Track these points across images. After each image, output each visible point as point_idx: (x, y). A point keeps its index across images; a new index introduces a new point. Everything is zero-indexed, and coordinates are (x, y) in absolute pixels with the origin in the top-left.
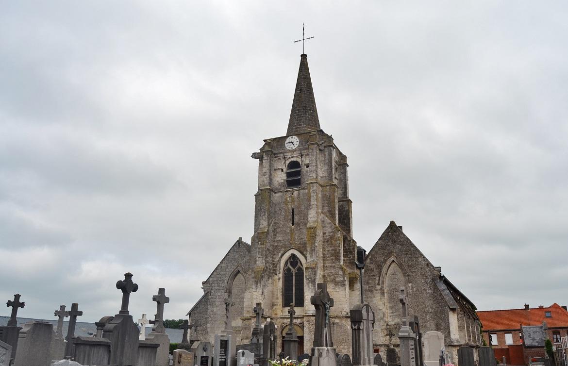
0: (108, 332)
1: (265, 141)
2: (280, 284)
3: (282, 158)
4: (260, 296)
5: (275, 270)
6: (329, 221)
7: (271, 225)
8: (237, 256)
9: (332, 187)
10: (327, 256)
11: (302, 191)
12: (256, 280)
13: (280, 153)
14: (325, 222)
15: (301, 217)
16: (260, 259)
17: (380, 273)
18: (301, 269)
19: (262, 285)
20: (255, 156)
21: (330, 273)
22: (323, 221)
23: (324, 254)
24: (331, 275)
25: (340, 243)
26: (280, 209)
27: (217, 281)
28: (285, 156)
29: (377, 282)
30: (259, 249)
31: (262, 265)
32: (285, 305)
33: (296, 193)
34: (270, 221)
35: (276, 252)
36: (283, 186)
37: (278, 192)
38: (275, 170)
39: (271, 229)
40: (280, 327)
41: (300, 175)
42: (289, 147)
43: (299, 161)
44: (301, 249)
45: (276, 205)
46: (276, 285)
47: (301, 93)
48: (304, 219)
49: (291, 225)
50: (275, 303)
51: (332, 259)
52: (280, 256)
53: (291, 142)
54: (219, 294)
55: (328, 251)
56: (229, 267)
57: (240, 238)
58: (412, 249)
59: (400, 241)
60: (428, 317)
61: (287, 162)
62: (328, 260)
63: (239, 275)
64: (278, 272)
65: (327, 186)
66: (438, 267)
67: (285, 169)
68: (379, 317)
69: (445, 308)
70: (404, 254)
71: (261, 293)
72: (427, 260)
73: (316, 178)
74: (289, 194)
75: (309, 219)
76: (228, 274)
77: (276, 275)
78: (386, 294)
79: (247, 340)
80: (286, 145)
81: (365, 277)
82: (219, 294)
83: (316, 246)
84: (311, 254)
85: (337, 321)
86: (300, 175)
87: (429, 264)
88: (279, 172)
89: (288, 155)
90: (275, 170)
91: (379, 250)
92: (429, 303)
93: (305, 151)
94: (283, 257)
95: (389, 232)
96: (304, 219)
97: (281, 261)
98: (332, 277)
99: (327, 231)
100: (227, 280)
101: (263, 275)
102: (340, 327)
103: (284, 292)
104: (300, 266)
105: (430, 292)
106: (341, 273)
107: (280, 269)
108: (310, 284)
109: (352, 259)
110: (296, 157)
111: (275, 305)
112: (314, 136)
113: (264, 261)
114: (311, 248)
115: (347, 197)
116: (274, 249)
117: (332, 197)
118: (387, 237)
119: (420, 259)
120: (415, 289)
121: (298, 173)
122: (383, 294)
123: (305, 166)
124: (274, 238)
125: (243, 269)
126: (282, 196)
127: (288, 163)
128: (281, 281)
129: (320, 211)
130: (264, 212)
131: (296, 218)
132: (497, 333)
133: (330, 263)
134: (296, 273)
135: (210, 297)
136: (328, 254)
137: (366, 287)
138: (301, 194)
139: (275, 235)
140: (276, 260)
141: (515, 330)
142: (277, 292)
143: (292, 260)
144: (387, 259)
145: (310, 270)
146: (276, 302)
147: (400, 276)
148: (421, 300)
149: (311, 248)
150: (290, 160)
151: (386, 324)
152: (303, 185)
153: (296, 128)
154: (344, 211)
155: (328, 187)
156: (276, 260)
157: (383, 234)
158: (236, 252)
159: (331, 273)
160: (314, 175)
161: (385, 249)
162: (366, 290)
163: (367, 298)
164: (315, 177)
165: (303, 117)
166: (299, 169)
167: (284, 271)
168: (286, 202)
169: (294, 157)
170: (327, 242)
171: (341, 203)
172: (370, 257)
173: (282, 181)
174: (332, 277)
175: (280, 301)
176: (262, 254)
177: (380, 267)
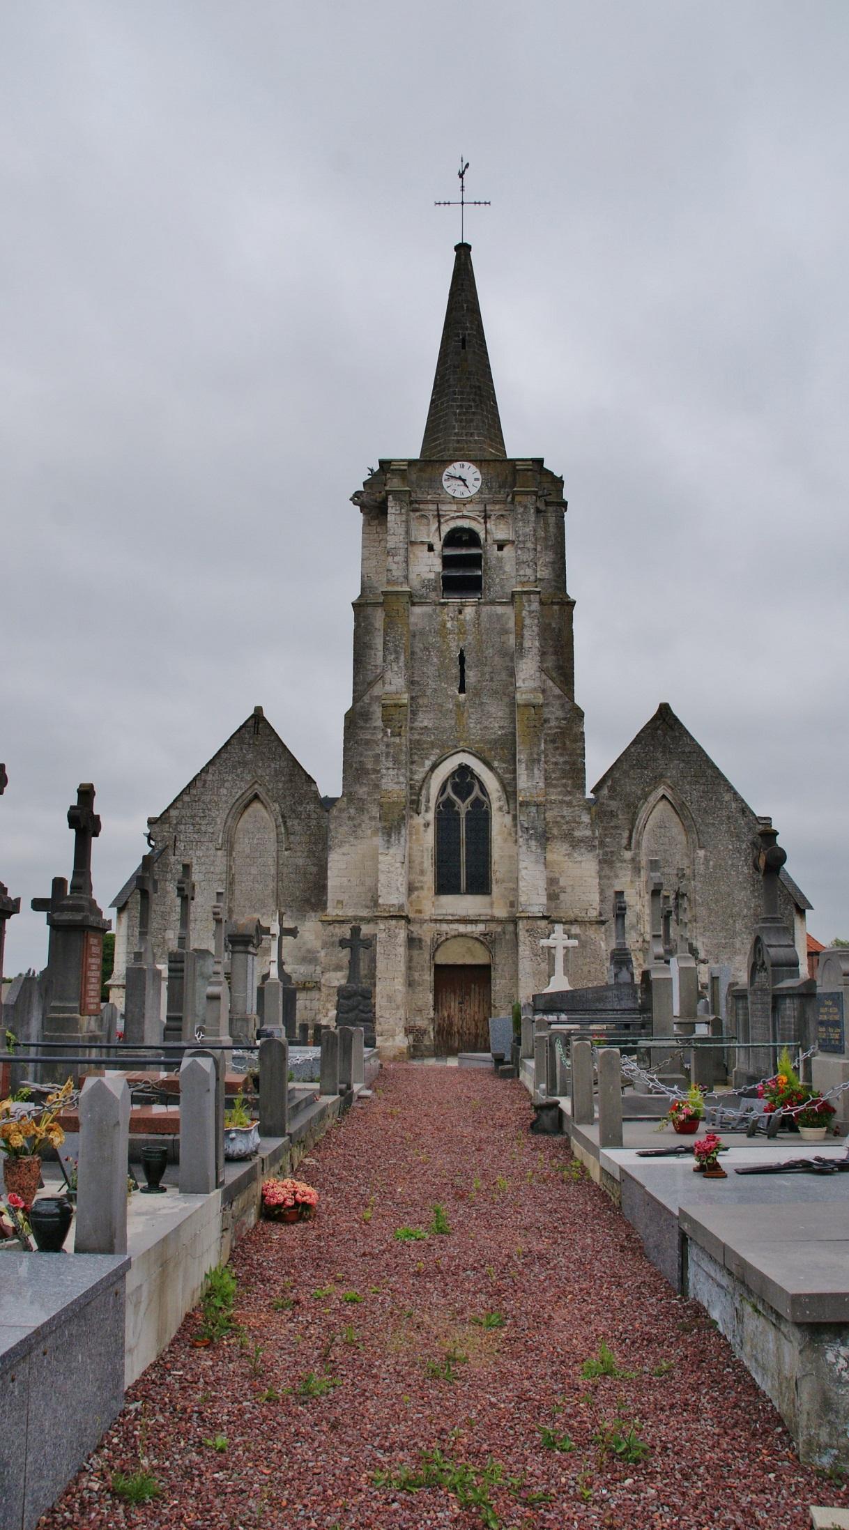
0: (786, 966)
2: (429, 838)
3: (430, 514)
6: (557, 691)
8: (250, 756)
10: (554, 776)
11: (486, 609)
12: (387, 824)
13: (426, 502)
15: (483, 674)
16: (391, 772)
17: (632, 822)
18: (483, 803)
19: (402, 840)
21: (559, 819)
24: (563, 821)
26: (426, 649)
27: (193, 817)
28: (441, 513)
29: (624, 842)
31: (397, 787)
33: (469, 612)
36: (435, 589)
37: (421, 604)
40: (429, 943)
41: (479, 566)
42: (452, 489)
44: (487, 754)
46: (417, 840)
47: (464, 347)
48: (492, 680)
50: (417, 885)
51: (565, 786)
52: (427, 768)
53: (460, 478)
55: (556, 764)
57: (258, 710)
58: (709, 772)
59: (683, 752)
60: (739, 926)
61: (446, 529)
63: (256, 806)
64: (423, 808)
65: (553, 603)
66: (765, 818)
67: (438, 546)
69: (786, 909)
70: (690, 783)
72: (743, 801)
74: (451, 611)
77: (418, 814)
78: (642, 873)
79: (340, 974)
80: (445, 484)
82: (199, 853)
84: (529, 769)
86: (479, 566)
87: (745, 810)
88: (422, 552)
91: (632, 767)
92: (742, 895)
93: (497, 507)
95: (657, 729)
96: (492, 680)
98: (565, 827)
99: (553, 717)
104: (480, 794)
105: (746, 871)
107: (428, 801)
108: (533, 843)
111: (417, 889)
114: (531, 754)
118: (653, 739)
119: (727, 797)
120: (711, 863)
121: (476, 561)
123: (496, 547)
125: (269, 790)
126: (431, 616)
127: (448, 530)
128: (432, 829)
130: (396, 652)
131: (471, 676)
133: (559, 794)
134: (468, 813)
136: (553, 772)
138: (483, 615)
140: (416, 777)
142: (423, 857)
143: (457, 780)
144: (650, 793)
145: (533, 809)
146: (422, 882)
147: (676, 830)
148: (724, 888)
149: (531, 754)
151: (641, 940)
152: (491, 595)
153: (458, 441)
155: (556, 607)
156: (416, 777)
157: (642, 731)
158: (249, 744)
159: (563, 817)
161: (645, 768)
166: (480, 551)
168: (442, 632)
169: (463, 517)
172: (609, 783)
173: (432, 576)
174: (565, 827)
175: (429, 879)
176: (396, 761)
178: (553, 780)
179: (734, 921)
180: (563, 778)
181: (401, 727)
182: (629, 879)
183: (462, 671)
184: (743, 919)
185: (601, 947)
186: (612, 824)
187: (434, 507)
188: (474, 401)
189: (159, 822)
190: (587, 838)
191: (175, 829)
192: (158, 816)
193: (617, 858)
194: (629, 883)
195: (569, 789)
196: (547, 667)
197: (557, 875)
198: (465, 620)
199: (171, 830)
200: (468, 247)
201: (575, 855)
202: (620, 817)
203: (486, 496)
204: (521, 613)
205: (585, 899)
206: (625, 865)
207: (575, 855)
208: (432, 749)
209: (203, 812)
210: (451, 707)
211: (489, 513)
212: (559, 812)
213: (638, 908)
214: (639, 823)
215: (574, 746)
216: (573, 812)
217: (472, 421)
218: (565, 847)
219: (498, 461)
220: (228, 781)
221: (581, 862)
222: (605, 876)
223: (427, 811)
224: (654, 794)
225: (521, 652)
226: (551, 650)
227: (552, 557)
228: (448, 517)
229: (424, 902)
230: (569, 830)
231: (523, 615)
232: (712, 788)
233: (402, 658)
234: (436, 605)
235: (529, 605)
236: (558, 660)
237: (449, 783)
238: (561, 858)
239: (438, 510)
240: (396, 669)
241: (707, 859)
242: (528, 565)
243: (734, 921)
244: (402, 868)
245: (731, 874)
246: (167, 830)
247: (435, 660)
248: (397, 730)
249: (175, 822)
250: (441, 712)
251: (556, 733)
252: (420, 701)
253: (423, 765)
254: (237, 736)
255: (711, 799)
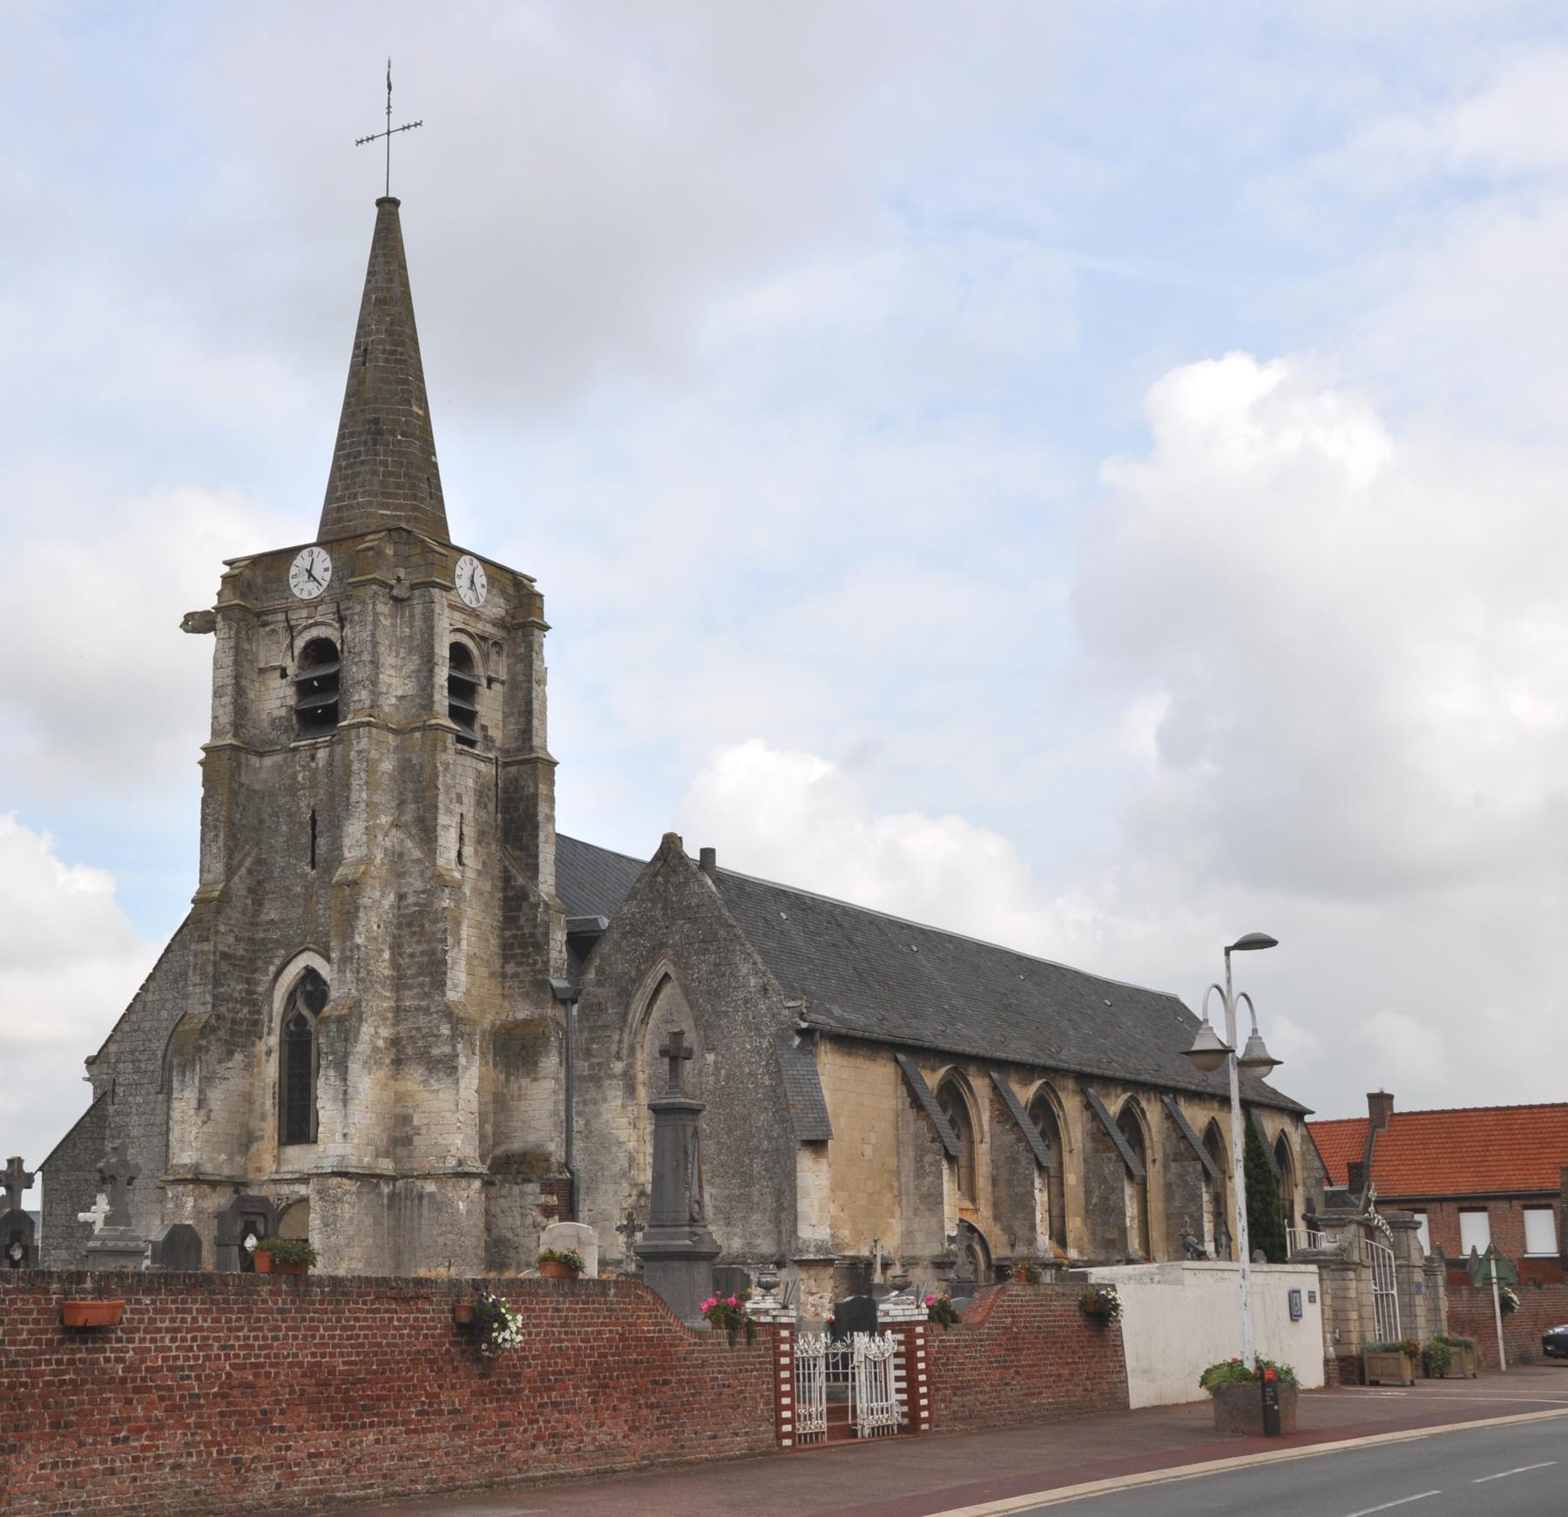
1: (227, 563)
2: (271, 1070)
4: (192, 1112)
5: (256, 1023)
6: (417, 854)
7: (243, 871)
9: (430, 734)
10: (409, 972)
13: (274, 612)
14: (406, 857)
16: (198, 989)
17: (624, 1018)
20: (196, 623)
21: (414, 1032)
22: (401, 855)
23: (395, 965)
24: (418, 1036)
25: (446, 930)
26: (275, 814)
28: (292, 623)
29: (614, 1047)
30: (196, 955)
31: (202, 1009)
32: (284, 1140)
33: (322, 754)
34: (238, 857)
35: (260, 963)
36: (286, 731)
38: (262, 671)
39: (239, 884)
43: (332, 638)
45: (263, 798)
46: (259, 1073)
47: (364, 364)
49: (308, 869)
50: (259, 1133)
51: (421, 985)
52: (271, 975)
54: (139, 1099)
55: (412, 956)
56: (169, 1005)
59: (689, 907)
60: (757, 1167)
61: (300, 643)
62: (410, 988)
64: (266, 1030)
68: (616, 1168)
71: (194, 1103)
73: (372, 707)
74: (303, 757)
75: (346, 854)
76: (166, 1029)
81: (581, 1031)
82: (139, 1099)
83: (358, 947)
85: (430, 1187)
88: (275, 681)
89: (300, 617)
90: (262, 671)
94: (280, 979)
95: (656, 875)
97: (276, 992)
99: (411, 891)
100: (163, 1047)
101: (203, 1043)
102: (440, 1205)
103: (285, 1094)
106: (445, 1030)
107: (271, 1020)
109: (540, 972)
110: (323, 624)
112: (371, 553)
113: (209, 998)
114: (344, 951)
115: (532, 749)
116: (254, 952)
117: (428, 770)
120: (723, 1072)
121: (332, 683)
122: (630, 1090)
124: (257, 913)
128: (275, 1057)
129: (384, 820)
130: (216, 827)
132: (1491, 1204)
133: (414, 997)
135: (111, 1109)
137: (582, 1066)
139: (258, 903)
141: (1441, 1200)
142: (264, 1095)
144: (648, 970)
150: (308, 636)
151: (635, 1193)
154: (521, 799)
155: (417, 735)
156: (260, 989)
159: (419, 1029)
160: (364, 694)
161: (641, 935)
162: (582, 1078)
163: (585, 1103)
164: (368, 703)
165: (362, 463)
167: (285, 1024)
168: (292, 789)
169: (317, 624)
170: (410, 925)
171: (514, 769)
173: (283, 712)
174: (420, 1043)
175: (269, 1127)
176: (203, 974)
177: (625, 995)
178: (408, 978)
179: (751, 1160)
180: (420, 974)
181: (209, 929)
182: (619, 1102)
183: (314, 837)
184: (763, 1157)
185: (459, 1209)
186: (600, 1023)
187: (281, 617)
188: (365, 443)
189: (98, 1061)
190: (446, 1056)
191: (115, 1069)
192: (95, 1053)
193: (606, 1073)
194: (619, 1109)
195: (426, 989)
196: (406, 821)
197: (410, 1111)
198: (317, 769)
199: (110, 1072)
200: (395, 203)
201: (432, 1081)
202: (610, 1011)
203: (337, 591)
204: (349, 755)
205: (443, 1142)
206: (615, 1082)
207: (432, 1081)
208: (277, 949)
209: (143, 1045)
210: (299, 889)
211: (343, 613)
212: (414, 1023)
213: (632, 1145)
214: (634, 1017)
215: (434, 928)
216: (430, 1021)
217: (357, 474)
218: (420, 1071)
219: (350, 538)
220: (168, 1000)
221: (438, 1091)
222: (591, 1100)
223: (269, 1034)
224: (651, 974)
225: (348, 810)
226: (410, 796)
227: (417, 662)
228: (300, 627)
229: (265, 1156)
230: (425, 1047)
231: (351, 758)
232: (726, 958)
233: (222, 835)
234: (286, 752)
235: (359, 743)
236: (418, 808)
237: (298, 994)
238: (415, 1087)
239: (287, 620)
240: (215, 851)
241: (717, 1068)
242: (364, 686)
243: (751, 1160)
244: (197, 1115)
245: (747, 1088)
246: (105, 1071)
247: (284, 828)
248: (205, 933)
249: (113, 1060)
250: (288, 898)
251: (414, 912)
252: (268, 886)
253: (266, 972)
254: (178, 938)
255: (724, 975)
